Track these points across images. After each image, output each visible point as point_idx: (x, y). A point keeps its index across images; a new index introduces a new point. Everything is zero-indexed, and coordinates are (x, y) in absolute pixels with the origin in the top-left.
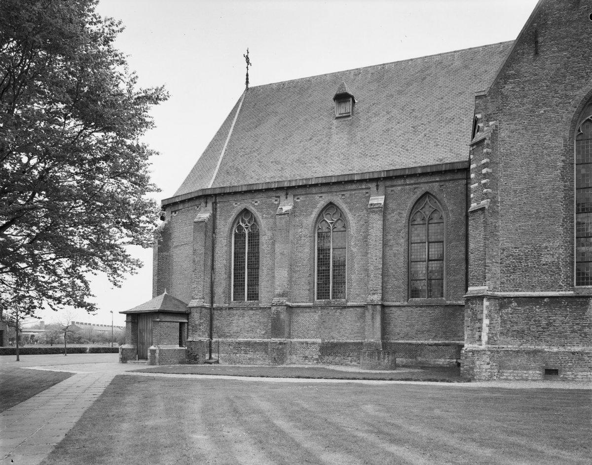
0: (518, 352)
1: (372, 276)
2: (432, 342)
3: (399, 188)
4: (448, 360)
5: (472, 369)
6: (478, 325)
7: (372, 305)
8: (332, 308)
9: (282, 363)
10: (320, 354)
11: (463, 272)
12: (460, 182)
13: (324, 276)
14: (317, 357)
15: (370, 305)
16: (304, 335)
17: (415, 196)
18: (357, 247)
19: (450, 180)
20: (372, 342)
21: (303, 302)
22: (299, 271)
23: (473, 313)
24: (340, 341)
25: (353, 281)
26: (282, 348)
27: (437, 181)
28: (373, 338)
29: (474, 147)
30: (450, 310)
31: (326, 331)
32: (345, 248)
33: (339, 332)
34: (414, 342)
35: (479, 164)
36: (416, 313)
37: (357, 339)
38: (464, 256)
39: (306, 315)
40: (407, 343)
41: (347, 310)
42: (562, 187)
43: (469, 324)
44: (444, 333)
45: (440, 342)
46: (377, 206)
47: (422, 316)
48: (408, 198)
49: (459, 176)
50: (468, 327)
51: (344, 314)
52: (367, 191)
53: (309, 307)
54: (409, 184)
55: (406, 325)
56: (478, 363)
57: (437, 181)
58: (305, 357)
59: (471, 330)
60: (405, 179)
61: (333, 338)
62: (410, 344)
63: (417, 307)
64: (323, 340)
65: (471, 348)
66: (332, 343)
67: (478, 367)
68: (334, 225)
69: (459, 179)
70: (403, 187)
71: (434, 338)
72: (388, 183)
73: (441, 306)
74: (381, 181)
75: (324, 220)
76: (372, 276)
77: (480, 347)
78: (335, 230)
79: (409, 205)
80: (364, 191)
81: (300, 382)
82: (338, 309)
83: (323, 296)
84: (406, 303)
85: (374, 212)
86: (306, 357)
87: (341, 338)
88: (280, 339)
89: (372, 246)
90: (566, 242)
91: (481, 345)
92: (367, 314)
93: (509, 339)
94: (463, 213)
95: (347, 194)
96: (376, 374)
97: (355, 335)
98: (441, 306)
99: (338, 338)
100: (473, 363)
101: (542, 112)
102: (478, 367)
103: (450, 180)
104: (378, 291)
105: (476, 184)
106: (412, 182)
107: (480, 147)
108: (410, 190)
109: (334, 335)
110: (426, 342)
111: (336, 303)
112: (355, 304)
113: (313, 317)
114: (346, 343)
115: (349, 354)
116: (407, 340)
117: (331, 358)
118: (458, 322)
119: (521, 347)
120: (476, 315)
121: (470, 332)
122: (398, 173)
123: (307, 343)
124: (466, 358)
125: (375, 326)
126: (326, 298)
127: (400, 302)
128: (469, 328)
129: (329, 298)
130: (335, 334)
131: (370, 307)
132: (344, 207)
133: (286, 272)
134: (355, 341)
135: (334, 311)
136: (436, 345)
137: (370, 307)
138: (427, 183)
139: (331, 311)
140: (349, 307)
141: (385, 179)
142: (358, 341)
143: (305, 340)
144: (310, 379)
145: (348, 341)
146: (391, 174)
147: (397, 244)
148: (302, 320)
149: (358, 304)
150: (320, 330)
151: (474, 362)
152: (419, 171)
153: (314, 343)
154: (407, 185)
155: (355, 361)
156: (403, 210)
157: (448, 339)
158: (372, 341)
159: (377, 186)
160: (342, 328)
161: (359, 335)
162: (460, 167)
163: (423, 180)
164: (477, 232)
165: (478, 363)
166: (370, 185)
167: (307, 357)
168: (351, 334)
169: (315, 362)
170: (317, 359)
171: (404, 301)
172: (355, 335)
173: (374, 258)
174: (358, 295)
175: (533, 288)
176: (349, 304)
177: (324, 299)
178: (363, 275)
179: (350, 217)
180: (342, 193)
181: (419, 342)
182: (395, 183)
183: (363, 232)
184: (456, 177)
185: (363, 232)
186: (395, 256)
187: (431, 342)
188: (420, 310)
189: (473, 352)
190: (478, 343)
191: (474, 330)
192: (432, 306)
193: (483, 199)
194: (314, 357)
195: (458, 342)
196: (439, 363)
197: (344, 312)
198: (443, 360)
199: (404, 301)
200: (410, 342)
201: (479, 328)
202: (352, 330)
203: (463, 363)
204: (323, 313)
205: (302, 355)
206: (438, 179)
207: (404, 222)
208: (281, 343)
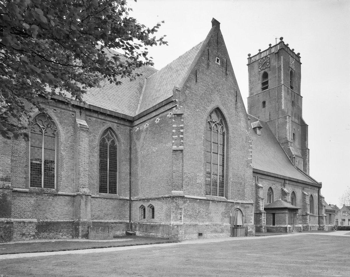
0: (190, 225)
1: (82, 175)
2: (113, 221)
3: (94, 119)
4: (122, 232)
5: (177, 235)
6: (180, 211)
7: (86, 195)
8: (46, 195)
9: (10, 241)
10: (36, 231)
11: (128, 180)
12: (127, 127)
13: (36, 168)
14: (34, 234)
15: (84, 195)
16: (20, 216)
17: (103, 128)
18: (65, 152)
19: (123, 125)
20: (85, 221)
21: (19, 188)
22: (16, 161)
23: (177, 205)
24: (53, 221)
25: (62, 176)
26: (10, 227)
27: (116, 123)
28: (86, 218)
29: (176, 116)
30: (122, 202)
31: (41, 213)
32: (55, 150)
33: (52, 214)
34: (103, 221)
35: (178, 126)
36: (104, 202)
37: (66, 219)
38: (129, 171)
39: (22, 199)
40: (99, 222)
41: (58, 197)
42: (203, 149)
43: (174, 211)
44: (119, 215)
45: (117, 221)
46: (85, 127)
47: (107, 205)
48: (99, 127)
49: (127, 124)
50: (173, 212)
51: (56, 200)
52: (73, 113)
53: (26, 193)
54: (100, 119)
55: (98, 210)
56: (180, 231)
57: (116, 123)
58: (23, 234)
59: (175, 214)
60: (98, 114)
61: (47, 219)
62: (101, 223)
63: (104, 198)
64: (38, 219)
65: (176, 224)
66: (47, 222)
67: (181, 233)
68: (45, 131)
69: (127, 126)
70: (96, 119)
71: (114, 218)
72: (88, 113)
73: (117, 199)
74: (83, 110)
75: (37, 124)
76: (82, 175)
77: (181, 223)
78: (46, 134)
79: (100, 132)
80: (71, 113)
81: (143, 247)
82: (51, 196)
83: (36, 184)
84: (98, 196)
85: (83, 130)
86: (23, 235)
87: (53, 219)
88: (6, 219)
89: (81, 154)
90: (204, 175)
91: (181, 222)
92: (82, 201)
93: (186, 219)
94: (128, 146)
95: (59, 110)
96: (122, 242)
97: (64, 216)
98: (117, 199)
99: (51, 218)
100: (178, 231)
101: (198, 111)
102: (181, 233)
103: (123, 125)
104: (86, 186)
105: (177, 136)
106: (103, 118)
107: (179, 117)
108: (101, 122)
109: (48, 216)
110: (110, 221)
111: (49, 191)
112: (64, 193)
113: (29, 201)
114: (58, 222)
115: (60, 231)
116: (98, 220)
117: (46, 234)
118: (126, 209)
119: (191, 223)
120: (179, 206)
121: (175, 215)
122: (96, 109)
123: (24, 222)
124: (173, 229)
125: (87, 210)
126: (38, 187)
127: (94, 194)
128: (174, 213)
129: (41, 187)
130: (48, 215)
131: (84, 197)
132: (55, 119)
133: (9, 159)
134: (65, 221)
135: (48, 197)
136: (115, 223)
137: (84, 197)
138: (111, 121)
139: (45, 197)
140: (59, 195)
141: (87, 109)
142: (66, 221)
143: (21, 220)
144: (8, 255)
145: (59, 220)
146: (92, 108)
147: (93, 156)
148: (19, 203)
149: (67, 193)
150: (35, 211)
151: (178, 231)
152: (108, 113)
153: (30, 223)
154: (99, 118)
155: (65, 235)
156: (96, 134)
157: (121, 219)
158: (85, 220)
159: (80, 112)
160: (54, 211)
161: (67, 216)
162: (129, 119)
163: (109, 119)
164: (177, 162)
165: (180, 231)
166: (75, 110)
167: (24, 234)
168: (61, 215)
169: (32, 237)
170: (34, 236)
171: (97, 194)
172: (64, 216)
173: (83, 163)
174: (66, 187)
175: (194, 194)
176: (60, 193)
177: (36, 187)
178: (70, 173)
179: (60, 127)
180: (55, 108)
181: (106, 221)
182: (92, 114)
183: (70, 142)
184: (125, 124)
185: (70, 142)
186: (91, 164)
187: (112, 221)
188: (106, 201)
189: (178, 226)
190: (179, 221)
191: (177, 214)
192: (112, 199)
193: (181, 145)
194: (31, 234)
195: (126, 221)
196: (117, 234)
197: (56, 198)
198: (119, 232)
199: (97, 194)
200: (100, 221)
201: (180, 213)
202: (62, 213)
203: (171, 232)
204: (38, 198)
205: (19, 233)
206: (116, 122)
207: (97, 142)
208: (8, 223)
